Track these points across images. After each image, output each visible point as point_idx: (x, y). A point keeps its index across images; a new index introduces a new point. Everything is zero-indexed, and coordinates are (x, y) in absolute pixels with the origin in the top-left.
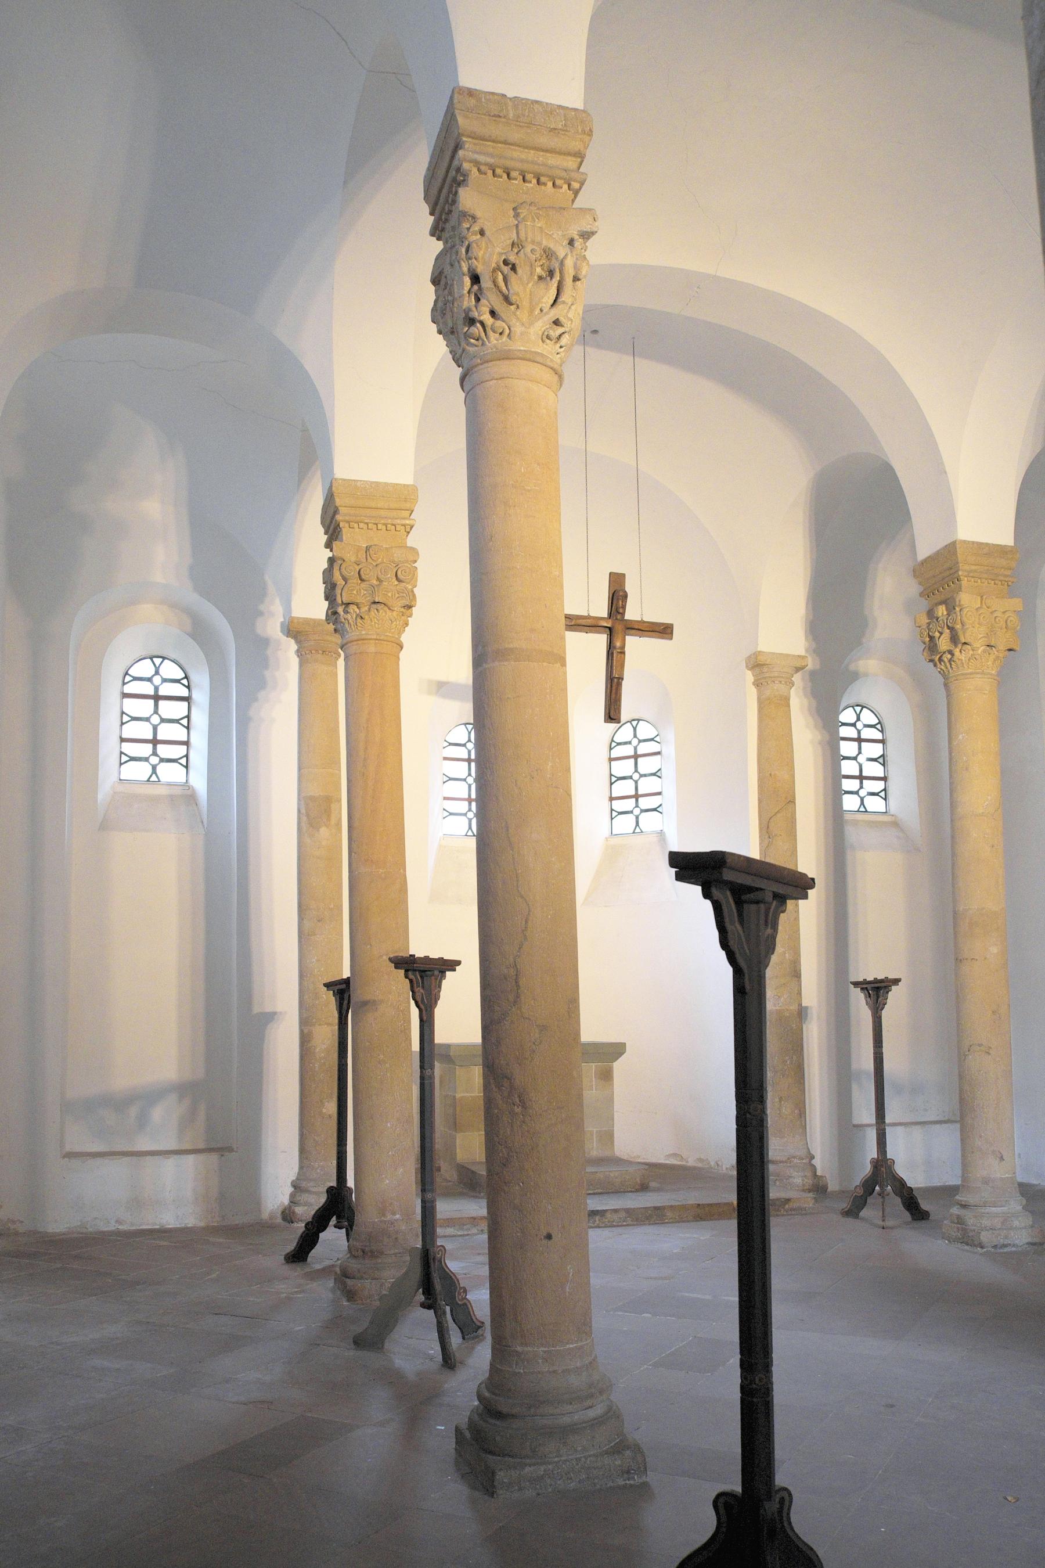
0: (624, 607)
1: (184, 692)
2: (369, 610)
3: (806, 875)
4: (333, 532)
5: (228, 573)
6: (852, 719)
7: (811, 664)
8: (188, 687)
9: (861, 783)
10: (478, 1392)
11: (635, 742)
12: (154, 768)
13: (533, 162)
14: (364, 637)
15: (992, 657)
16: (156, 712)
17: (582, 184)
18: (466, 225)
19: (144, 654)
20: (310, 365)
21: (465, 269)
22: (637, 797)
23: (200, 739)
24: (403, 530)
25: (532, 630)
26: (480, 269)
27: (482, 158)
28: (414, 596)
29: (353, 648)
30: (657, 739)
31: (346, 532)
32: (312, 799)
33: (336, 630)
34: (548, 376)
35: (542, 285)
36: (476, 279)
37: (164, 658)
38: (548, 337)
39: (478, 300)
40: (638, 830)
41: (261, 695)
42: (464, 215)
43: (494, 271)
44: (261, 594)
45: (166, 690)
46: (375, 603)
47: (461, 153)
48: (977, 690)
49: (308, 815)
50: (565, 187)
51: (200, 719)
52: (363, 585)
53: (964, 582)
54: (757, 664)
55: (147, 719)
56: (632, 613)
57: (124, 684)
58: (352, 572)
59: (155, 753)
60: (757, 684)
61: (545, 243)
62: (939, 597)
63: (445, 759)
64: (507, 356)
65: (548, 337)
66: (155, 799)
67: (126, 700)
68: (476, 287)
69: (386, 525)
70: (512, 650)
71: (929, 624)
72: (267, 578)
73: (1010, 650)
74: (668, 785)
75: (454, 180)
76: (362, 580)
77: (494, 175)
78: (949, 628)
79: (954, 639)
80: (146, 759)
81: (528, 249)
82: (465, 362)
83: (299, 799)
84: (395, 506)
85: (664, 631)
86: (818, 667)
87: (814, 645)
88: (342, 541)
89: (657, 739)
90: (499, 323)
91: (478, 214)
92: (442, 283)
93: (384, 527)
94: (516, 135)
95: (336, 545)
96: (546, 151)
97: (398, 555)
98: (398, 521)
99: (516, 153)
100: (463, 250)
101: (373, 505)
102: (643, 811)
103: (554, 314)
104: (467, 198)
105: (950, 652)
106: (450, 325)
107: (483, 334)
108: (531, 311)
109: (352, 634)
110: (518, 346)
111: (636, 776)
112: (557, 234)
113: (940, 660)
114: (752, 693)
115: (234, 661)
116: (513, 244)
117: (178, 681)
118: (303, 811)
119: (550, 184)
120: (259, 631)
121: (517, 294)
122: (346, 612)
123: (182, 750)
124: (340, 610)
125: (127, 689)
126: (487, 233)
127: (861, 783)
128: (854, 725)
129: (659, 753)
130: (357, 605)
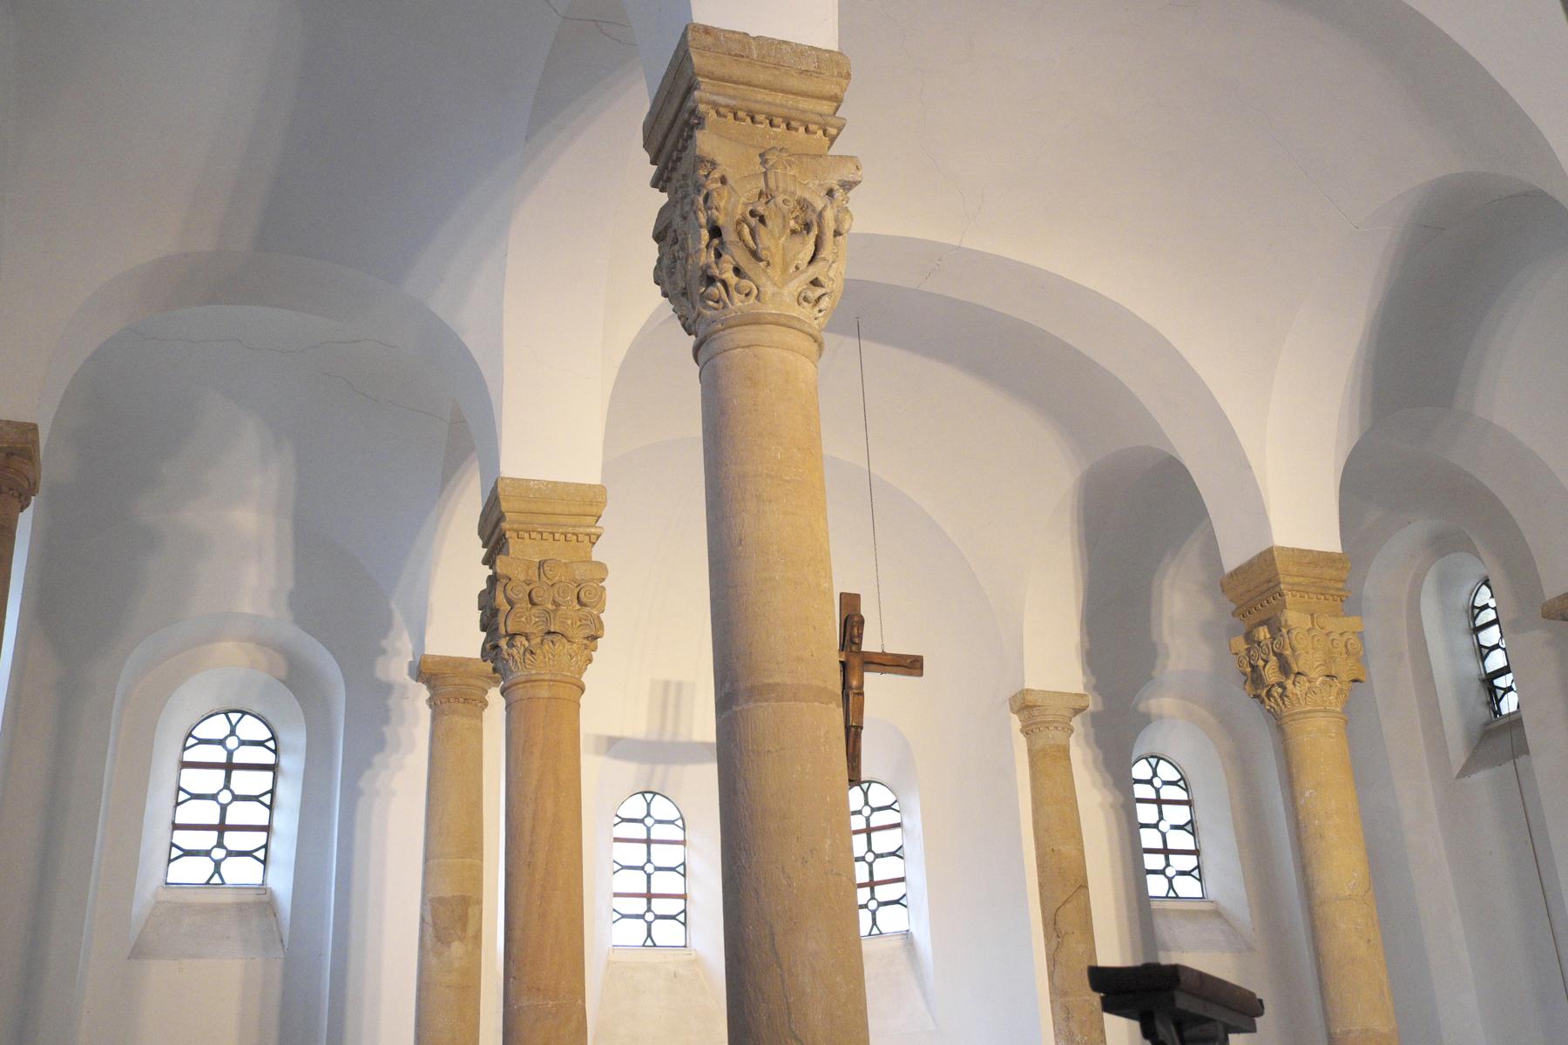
0: (860, 636)
1: (269, 758)
3: (1253, 995)
4: (494, 539)
5: (341, 597)
6: (1148, 775)
7: (1093, 703)
8: (275, 751)
9: (1167, 859)
11: (867, 811)
12: (218, 864)
13: (782, 106)
15: (1334, 690)
16: (227, 786)
17: (840, 130)
18: (703, 172)
19: (217, 707)
20: (472, 341)
21: (703, 220)
22: (649, 896)
23: (287, 822)
25: (799, 659)
26: (722, 221)
27: (721, 100)
28: (601, 623)
29: (519, 693)
30: (896, 806)
31: (513, 544)
32: (441, 901)
33: (495, 670)
34: (807, 344)
35: (797, 239)
36: (716, 232)
37: (244, 713)
38: (805, 299)
39: (718, 255)
40: (875, 931)
41: (378, 759)
42: (701, 160)
43: (738, 223)
44: (385, 626)
45: (244, 755)
46: (549, 633)
47: (697, 94)
48: (1319, 734)
49: (435, 924)
50: (820, 133)
51: (289, 794)
52: (535, 611)
53: (1288, 598)
54: (1026, 707)
55: (214, 797)
56: (870, 644)
57: (185, 749)
58: (519, 594)
59: (220, 844)
60: (1027, 731)
61: (799, 193)
62: (1255, 617)
63: (616, 840)
64: (756, 320)
65: (805, 299)
66: (216, 909)
67: (184, 771)
68: (716, 241)
70: (773, 687)
71: (1248, 650)
72: (393, 605)
73: (1355, 681)
74: (914, 868)
75: (687, 123)
76: (533, 604)
77: (736, 117)
78: (1275, 654)
79: (1285, 668)
80: (207, 853)
81: (779, 200)
82: (702, 330)
83: (423, 903)
84: (576, 511)
85: (911, 665)
86: (1100, 707)
87: (1094, 681)
88: (507, 554)
89: (896, 806)
90: (745, 283)
91: (718, 159)
92: (670, 235)
94: (762, 76)
95: (501, 561)
96: (798, 96)
97: (580, 572)
99: (763, 96)
100: (701, 199)
101: (549, 510)
102: (881, 904)
103: (813, 272)
104: (705, 142)
105: (1281, 685)
106: (681, 284)
107: (724, 295)
108: (785, 267)
109: (519, 674)
110: (770, 309)
111: (870, 857)
112: (813, 184)
113: (1269, 694)
114: (1021, 743)
115: (342, 717)
116: (761, 194)
117: (261, 743)
118: (429, 919)
119: (802, 129)
120: (380, 674)
121: (768, 249)
122: (511, 645)
123: (260, 838)
124: (503, 643)
125: (189, 756)
126: (730, 181)
127: (1167, 859)
128: (1150, 782)
129: (898, 825)
130: (527, 637)
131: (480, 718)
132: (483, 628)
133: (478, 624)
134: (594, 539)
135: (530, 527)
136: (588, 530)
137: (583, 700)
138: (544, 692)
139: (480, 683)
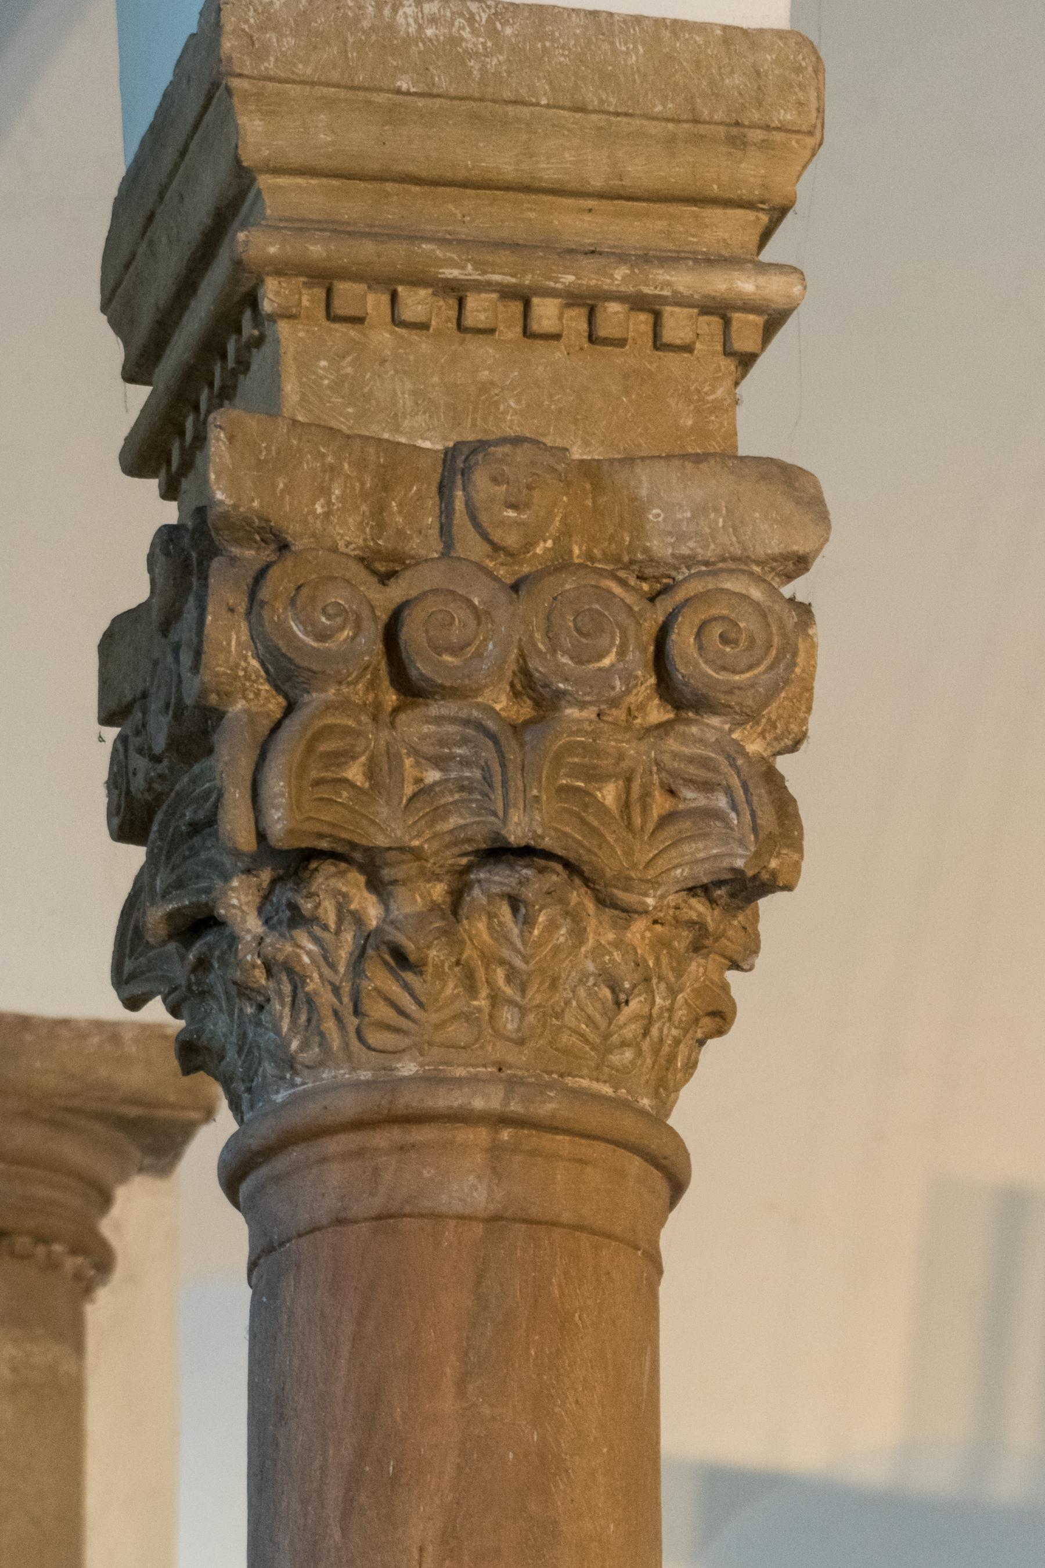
2: (457, 896)
10: (828, 528)
14: (410, 1099)
24: (708, 346)
28: (785, 807)
29: (325, 1183)
31: (304, 360)
33: (192, 1053)
46: (499, 853)
52: (419, 726)
69: (589, 304)
76: (411, 689)
88: (271, 404)
93: (576, 321)
97: (675, 515)
98: (682, 280)
101: (502, 160)
124: (240, 902)
131: (73, 1335)
132: (129, 822)
133: (97, 801)
134: (747, 330)
135: (395, 255)
136: (720, 283)
137: (679, 1236)
138: (465, 1183)
139: (72, 1151)
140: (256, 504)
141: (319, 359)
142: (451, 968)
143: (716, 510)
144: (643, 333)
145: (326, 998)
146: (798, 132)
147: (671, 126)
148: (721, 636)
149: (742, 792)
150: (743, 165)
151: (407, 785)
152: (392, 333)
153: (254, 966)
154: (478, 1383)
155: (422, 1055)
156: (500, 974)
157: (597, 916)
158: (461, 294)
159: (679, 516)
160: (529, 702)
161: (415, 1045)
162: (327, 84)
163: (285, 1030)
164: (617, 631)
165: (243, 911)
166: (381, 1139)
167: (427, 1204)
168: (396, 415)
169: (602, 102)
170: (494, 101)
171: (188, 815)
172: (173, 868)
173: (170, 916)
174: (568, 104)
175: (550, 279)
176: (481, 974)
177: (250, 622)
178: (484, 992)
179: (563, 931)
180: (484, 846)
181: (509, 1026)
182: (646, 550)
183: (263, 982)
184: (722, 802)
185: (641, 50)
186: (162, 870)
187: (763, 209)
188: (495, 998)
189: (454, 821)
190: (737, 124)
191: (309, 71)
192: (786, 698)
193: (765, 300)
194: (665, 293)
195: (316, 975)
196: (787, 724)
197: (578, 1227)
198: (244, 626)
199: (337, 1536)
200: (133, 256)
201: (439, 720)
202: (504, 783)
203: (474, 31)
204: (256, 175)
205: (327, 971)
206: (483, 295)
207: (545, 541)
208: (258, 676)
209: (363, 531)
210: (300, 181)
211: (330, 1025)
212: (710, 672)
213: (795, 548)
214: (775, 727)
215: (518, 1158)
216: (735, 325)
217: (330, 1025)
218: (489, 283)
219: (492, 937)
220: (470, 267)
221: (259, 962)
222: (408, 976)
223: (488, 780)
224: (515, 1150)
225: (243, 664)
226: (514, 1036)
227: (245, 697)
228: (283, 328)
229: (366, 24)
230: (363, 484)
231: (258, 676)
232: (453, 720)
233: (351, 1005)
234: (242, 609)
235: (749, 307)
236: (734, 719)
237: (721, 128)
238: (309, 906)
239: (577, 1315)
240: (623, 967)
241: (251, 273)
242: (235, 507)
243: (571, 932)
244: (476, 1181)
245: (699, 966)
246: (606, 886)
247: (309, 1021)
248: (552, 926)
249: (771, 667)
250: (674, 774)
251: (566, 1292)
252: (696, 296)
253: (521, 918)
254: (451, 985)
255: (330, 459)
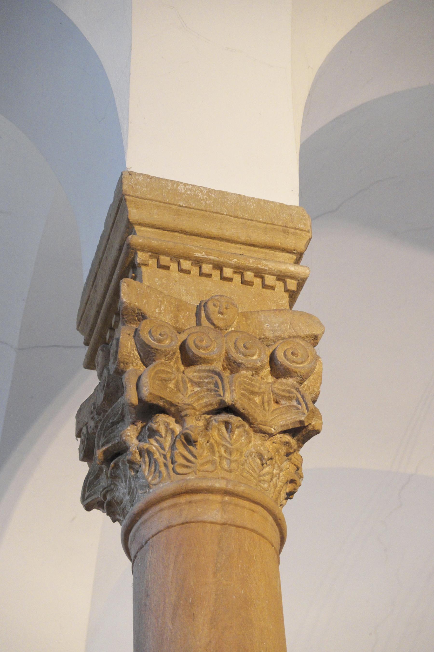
124: (130, 434)
140: (136, 304)
141: (155, 278)
142: (206, 445)
143: (287, 323)
144: (258, 284)
145: (161, 460)
146: (305, 231)
147: (265, 225)
148: (292, 353)
149: (301, 399)
150: (288, 239)
151: (189, 391)
152: (178, 274)
153: (136, 452)
154: (221, 573)
155: (196, 474)
156: (222, 450)
157: (254, 437)
158: (200, 264)
159: (275, 325)
160: (229, 371)
161: (194, 471)
162: (157, 201)
163: (146, 474)
164: (258, 350)
165: (131, 437)
166: (182, 499)
167: (200, 519)
168: (180, 295)
169: (243, 216)
170: (209, 212)
171: (111, 421)
172: (105, 437)
173: (105, 452)
174: (233, 215)
175: (229, 260)
176: (216, 448)
177: (135, 339)
178: (217, 455)
179: (243, 438)
180: (216, 407)
181: (226, 466)
182: (264, 335)
183: (139, 459)
184: (295, 403)
185: (255, 205)
186: (101, 439)
187: (294, 253)
188: (221, 457)
189: (205, 400)
190: (286, 226)
191: (151, 196)
192: (313, 379)
193: (297, 273)
194: (266, 268)
195: (158, 453)
196: (313, 388)
197: (252, 530)
198: (133, 340)
199: (170, 626)
200: (89, 296)
201: (200, 371)
202: (223, 387)
203: (202, 194)
204: (134, 226)
205: (162, 451)
206: (208, 265)
207: (231, 328)
208: (137, 357)
209: (172, 321)
210: (148, 229)
211: (163, 469)
212: (289, 363)
213: (314, 332)
214: (310, 389)
215: (231, 506)
216: (288, 283)
217: (163, 469)
218: (210, 260)
219: (219, 437)
220: (204, 253)
221: (137, 451)
222: (191, 447)
223: (216, 385)
224: (230, 503)
225: (132, 352)
226: (228, 469)
227: (133, 365)
228: (143, 268)
229: (169, 188)
230: (171, 308)
231: (137, 357)
232: (204, 371)
233: (170, 461)
234: (132, 335)
235: (292, 277)
236: (297, 379)
237: (281, 227)
238: (156, 426)
239: (254, 557)
240: (264, 451)
241: (133, 249)
242: (130, 304)
243: (246, 438)
244: (217, 513)
245: (287, 464)
246: (258, 424)
247: (155, 470)
248: (240, 436)
249: (309, 363)
250: (277, 395)
251: (250, 549)
252: (276, 270)
253: (229, 430)
254: (206, 451)
255: (160, 299)
